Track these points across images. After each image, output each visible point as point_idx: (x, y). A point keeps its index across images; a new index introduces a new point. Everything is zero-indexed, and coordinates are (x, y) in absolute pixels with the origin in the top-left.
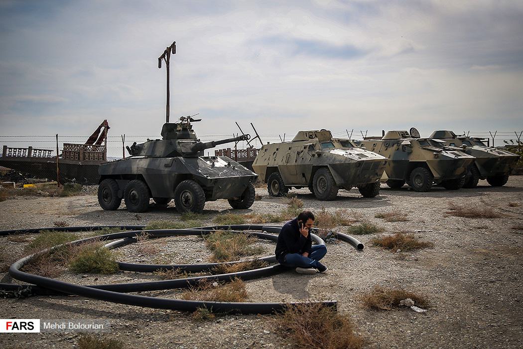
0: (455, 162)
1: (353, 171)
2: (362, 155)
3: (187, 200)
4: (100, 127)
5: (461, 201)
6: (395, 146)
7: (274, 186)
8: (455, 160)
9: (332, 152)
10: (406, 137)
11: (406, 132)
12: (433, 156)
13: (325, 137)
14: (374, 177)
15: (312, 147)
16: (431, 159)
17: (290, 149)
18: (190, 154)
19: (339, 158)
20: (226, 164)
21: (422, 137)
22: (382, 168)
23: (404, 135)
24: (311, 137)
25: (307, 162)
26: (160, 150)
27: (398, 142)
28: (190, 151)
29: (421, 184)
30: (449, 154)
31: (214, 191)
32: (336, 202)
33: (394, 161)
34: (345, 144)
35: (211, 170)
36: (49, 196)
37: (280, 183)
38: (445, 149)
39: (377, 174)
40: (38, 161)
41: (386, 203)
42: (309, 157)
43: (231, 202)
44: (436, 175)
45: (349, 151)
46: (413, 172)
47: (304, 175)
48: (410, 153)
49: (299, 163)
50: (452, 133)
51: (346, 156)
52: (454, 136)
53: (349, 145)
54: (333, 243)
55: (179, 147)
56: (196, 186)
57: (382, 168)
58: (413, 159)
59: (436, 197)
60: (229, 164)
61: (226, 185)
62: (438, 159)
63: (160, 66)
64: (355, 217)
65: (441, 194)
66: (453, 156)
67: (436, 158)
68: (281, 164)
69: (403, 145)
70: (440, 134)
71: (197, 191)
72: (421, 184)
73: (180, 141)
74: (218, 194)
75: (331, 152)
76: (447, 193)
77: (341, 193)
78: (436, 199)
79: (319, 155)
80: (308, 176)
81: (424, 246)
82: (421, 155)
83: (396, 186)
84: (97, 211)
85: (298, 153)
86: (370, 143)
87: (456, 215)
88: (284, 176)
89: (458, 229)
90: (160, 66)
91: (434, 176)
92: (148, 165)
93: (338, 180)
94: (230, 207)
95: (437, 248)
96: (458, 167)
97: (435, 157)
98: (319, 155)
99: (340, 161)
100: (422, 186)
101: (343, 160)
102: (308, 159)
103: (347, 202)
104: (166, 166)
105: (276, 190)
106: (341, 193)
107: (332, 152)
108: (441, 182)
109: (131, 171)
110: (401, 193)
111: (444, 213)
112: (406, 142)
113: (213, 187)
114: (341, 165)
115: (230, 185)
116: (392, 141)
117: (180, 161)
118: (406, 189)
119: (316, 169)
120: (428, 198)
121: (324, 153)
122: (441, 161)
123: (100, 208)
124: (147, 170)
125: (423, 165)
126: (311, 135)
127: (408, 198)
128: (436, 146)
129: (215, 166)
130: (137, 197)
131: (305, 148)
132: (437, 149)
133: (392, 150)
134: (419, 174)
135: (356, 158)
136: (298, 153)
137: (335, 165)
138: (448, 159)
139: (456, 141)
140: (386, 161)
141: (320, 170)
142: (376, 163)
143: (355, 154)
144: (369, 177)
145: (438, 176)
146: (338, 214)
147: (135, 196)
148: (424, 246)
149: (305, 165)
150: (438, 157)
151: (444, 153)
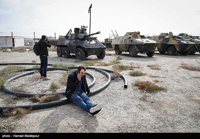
0: (187, 45)
1: (143, 47)
2: (148, 41)
3: (79, 55)
4: (69, 31)
5: (187, 61)
6: (163, 38)
7: (117, 51)
8: (186, 44)
9: (137, 40)
10: (167, 35)
11: (168, 33)
12: (177, 43)
13: (136, 34)
14: (152, 49)
15: (130, 38)
16: (177, 44)
17: (123, 38)
18: (83, 39)
19: (139, 42)
20: (95, 43)
21: (174, 35)
22: (155, 46)
23: (167, 34)
24: (130, 34)
25: (128, 43)
26: (73, 37)
27: (164, 37)
28: (83, 38)
29: (171, 53)
30: (185, 42)
31: (88, 52)
32: (136, 58)
33: (162, 44)
34: (143, 37)
35: (88, 45)
36: (52, 51)
37: (119, 51)
38: (182, 40)
39: (153, 48)
40: (52, 41)
41: (155, 60)
42: (128, 41)
43: (97, 56)
44: (178, 50)
45: (143, 40)
46: (169, 48)
47: (126, 48)
48: (168, 41)
49: (125, 43)
50: (187, 34)
51: (141, 41)
52: (187, 35)
53: (144, 37)
54: (116, 81)
55: (79, 36)
56: (81, 50)
57: (155, 46)
58: (169, 43)
59: (177, 58)
60: (96, 43)
61: (93, 51)
62: (179, 44)
63: (89, 13)
64: (137, 66)
65: (179, 57)
66: (186, 43)
67: (179, 43)
68: (119, 44)
69: (166, 38)
70: (182, 35)
71: (82, 52)
72: (171, 53)
73: (80, 34)
74: (90, 53)
75: (136, 40)
76: (182, 57)
77: (139, 54)
78: (176, 59)
79: (132, 41)
80: (128, 48)
81: (161, 89)
82: (172, 42)
83: (162, 53)
84: (57, 57)
85: (125, 40)
86: (154, 38)
87: (184, 68)
88: (120, 48)
89: (184, 77)
90: (89, 13)
91: (177, 50)
92: (69, 42)
93: (137, 50)
94: (97, 58)
95: (169, 92)
96: (187, 47)
97: (178, 43)
98: (132, 41)
99: (139, 43)
100: (172, 53)
101: (140, 42)
102: (128, 42)
103: (140, 58)
104: (73, 43)
105: (117, 52)
106: (139, 54)
107: (137, 40)
108: (179, 52)
109: (64, 44)
110: (163, 55)
111: (178, 66)
112: (167, 37)
113: (87, 51)
114: (139, 44)
115: (95, 50)
116: (162, 36)
117: (78, 41)
118: (166, 54)
119: (130, 46)
120: (173, 58)
121: (133, 40)
122: (180, 44)
123: (57, 56)
124: (68, 44)
125: (173, 45)
126: (131, 34)
127: (165, 58)
128: (179, 39)
129: (91, 43)
130: (66, 53)
131: (128, 38)
132: (179, 40)
133: (161, 40)
134: (171, 49)
135: (145, 42)
136: (125, 40)
137: (137, 44)
138: (184, 44)
139: (187, 37)
140: (157, 44)
141: (132, 46)
142: (153, 45)
143: (145, 41)
144: (150, 49)
145: (179, 50)
146: (131, 64)
147: (65, 53)
148: (161, 89)
149: (127, 44)
150: (179, 43)
151: (182, 41)
